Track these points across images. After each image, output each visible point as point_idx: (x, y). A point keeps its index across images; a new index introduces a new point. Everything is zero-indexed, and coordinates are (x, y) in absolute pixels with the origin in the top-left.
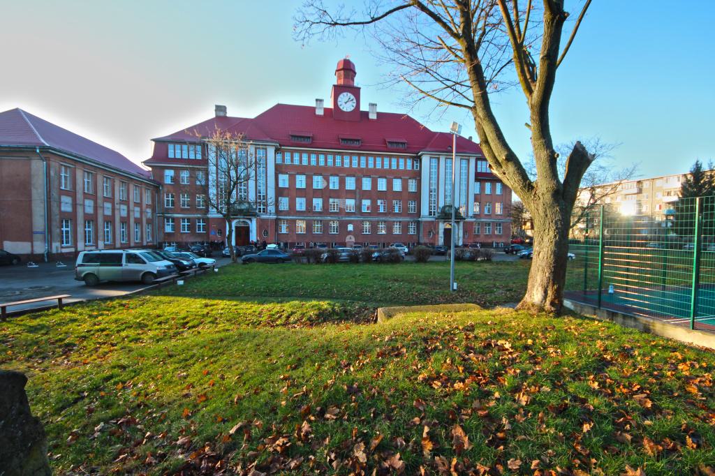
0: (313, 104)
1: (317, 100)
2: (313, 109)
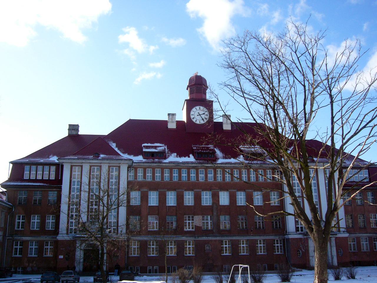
0: (165, 118)
1: (169, 114)
2: (165, 123)
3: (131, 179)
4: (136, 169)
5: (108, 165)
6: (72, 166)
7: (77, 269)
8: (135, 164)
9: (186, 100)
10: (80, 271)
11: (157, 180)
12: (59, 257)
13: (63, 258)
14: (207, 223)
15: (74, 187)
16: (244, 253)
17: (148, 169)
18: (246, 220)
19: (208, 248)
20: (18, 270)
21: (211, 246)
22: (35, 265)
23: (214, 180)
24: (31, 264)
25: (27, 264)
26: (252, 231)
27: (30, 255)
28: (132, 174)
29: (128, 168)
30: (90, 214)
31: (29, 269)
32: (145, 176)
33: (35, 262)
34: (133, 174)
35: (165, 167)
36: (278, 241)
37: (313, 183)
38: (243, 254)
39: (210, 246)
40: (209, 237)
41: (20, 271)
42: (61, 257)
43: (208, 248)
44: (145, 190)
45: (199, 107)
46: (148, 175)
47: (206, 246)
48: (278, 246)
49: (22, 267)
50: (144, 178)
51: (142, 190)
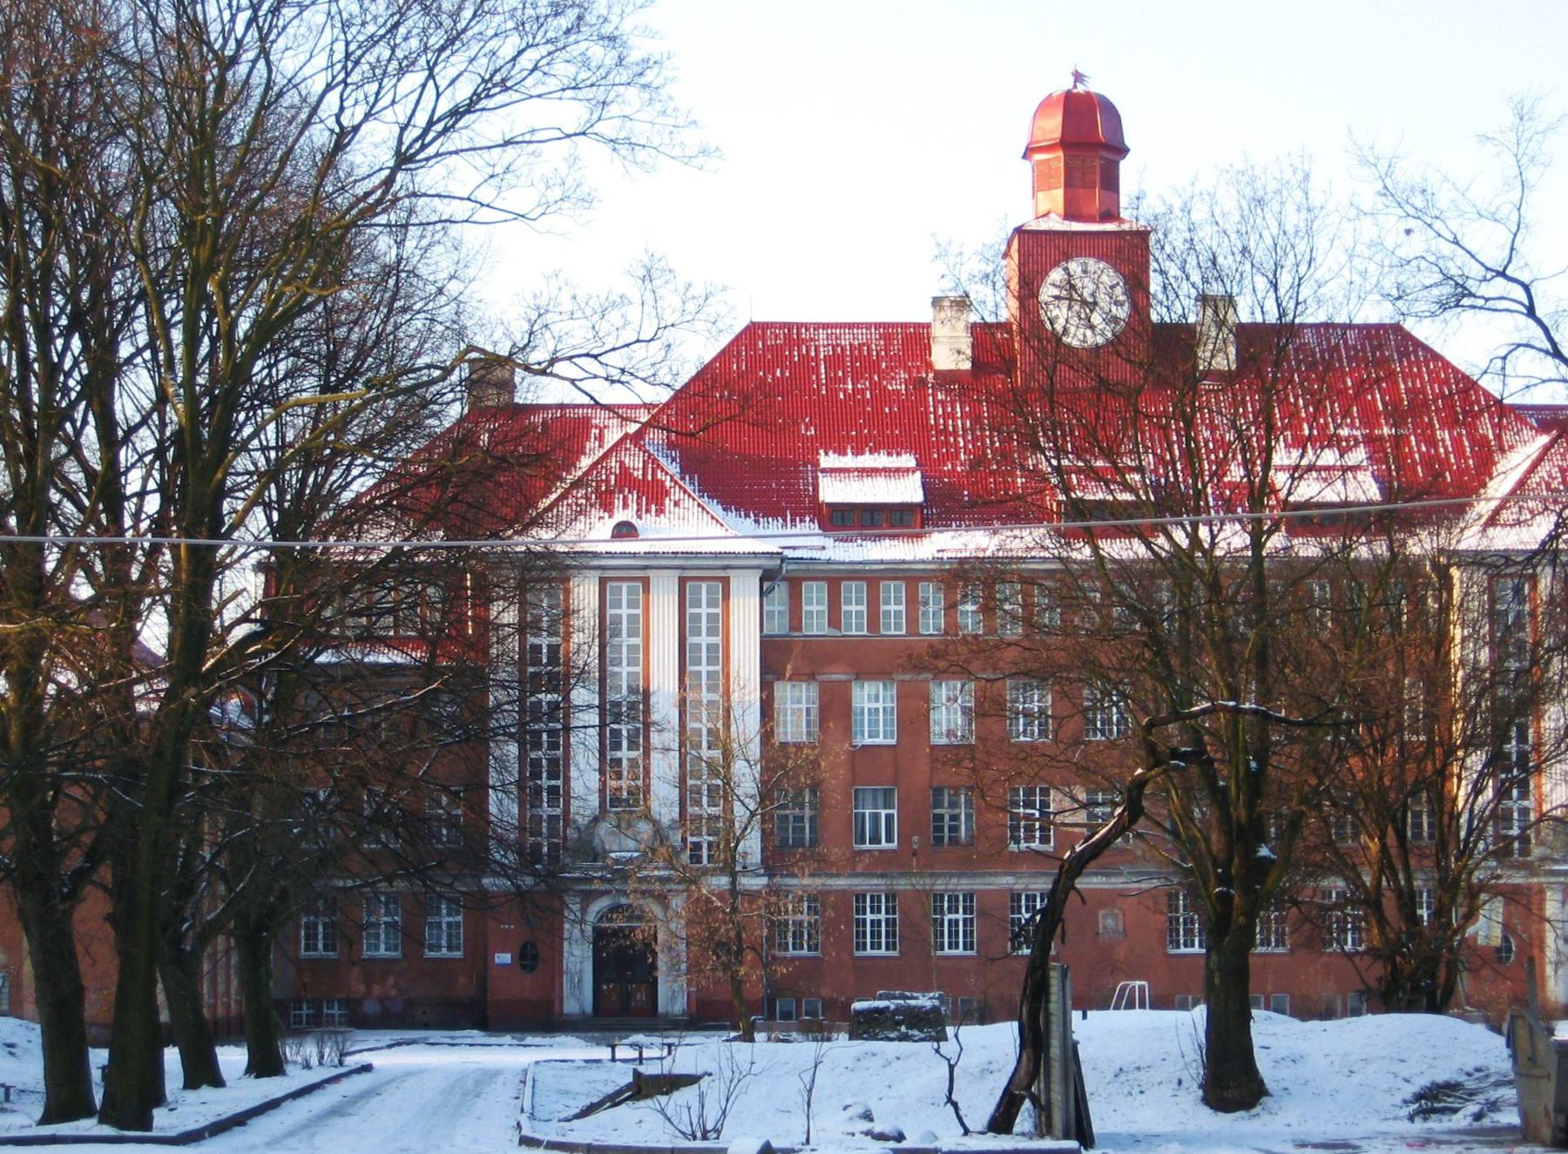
3: (778, 627)
4: (795, 584)
5: (677, 573)
6: (682, 582)
7: (571, 1006)
8: (792, 567)
9: (1019, 231)
10: (584, 1013)
11: (890, 629)
12: (497, 961)
13: (509, 961)
14: (955, 818)
15: (711, 668)
16: (957, 947)
17: (886, 582)
18: (815, 809)
19: (1110, 922)
20: (325, 1011)
21: (1124, 915)
22: (393, 992)
23: (909, 633)
24: (377, 989)
25: (362, 988)
26: (914, 854)
27: (306, 950)
28: (777, 608)
29: (762, 580)
30: (560, 783)
31: (371, 1007)
32: (834, 619)
33: (391, 980)
34: (782, 608)
35: (879, 575)
36: (879, 901)
37: (700, 635)
38: (797, 953)
39: (1121, 917)
40: (1113, 880)
41: (333, 1015)
42: (504, 958)
43: (1110, 922)
44: (834, 677)
45: (1082, 260)
46: (859, 608)
47: (1100, 917)
48: (954, 924)
49: (308, 1002)
50: (830, 625)
51: (824, 677)
